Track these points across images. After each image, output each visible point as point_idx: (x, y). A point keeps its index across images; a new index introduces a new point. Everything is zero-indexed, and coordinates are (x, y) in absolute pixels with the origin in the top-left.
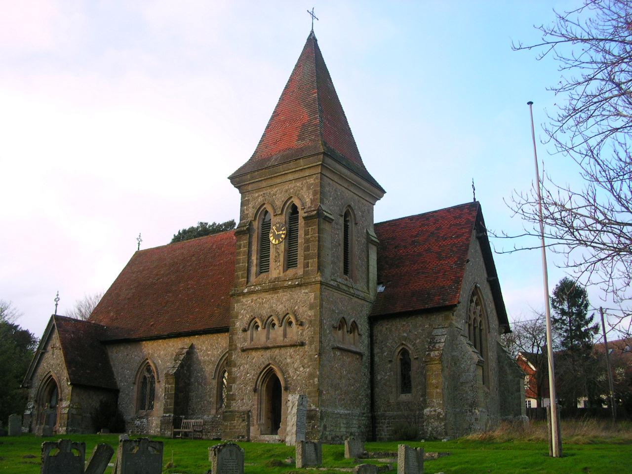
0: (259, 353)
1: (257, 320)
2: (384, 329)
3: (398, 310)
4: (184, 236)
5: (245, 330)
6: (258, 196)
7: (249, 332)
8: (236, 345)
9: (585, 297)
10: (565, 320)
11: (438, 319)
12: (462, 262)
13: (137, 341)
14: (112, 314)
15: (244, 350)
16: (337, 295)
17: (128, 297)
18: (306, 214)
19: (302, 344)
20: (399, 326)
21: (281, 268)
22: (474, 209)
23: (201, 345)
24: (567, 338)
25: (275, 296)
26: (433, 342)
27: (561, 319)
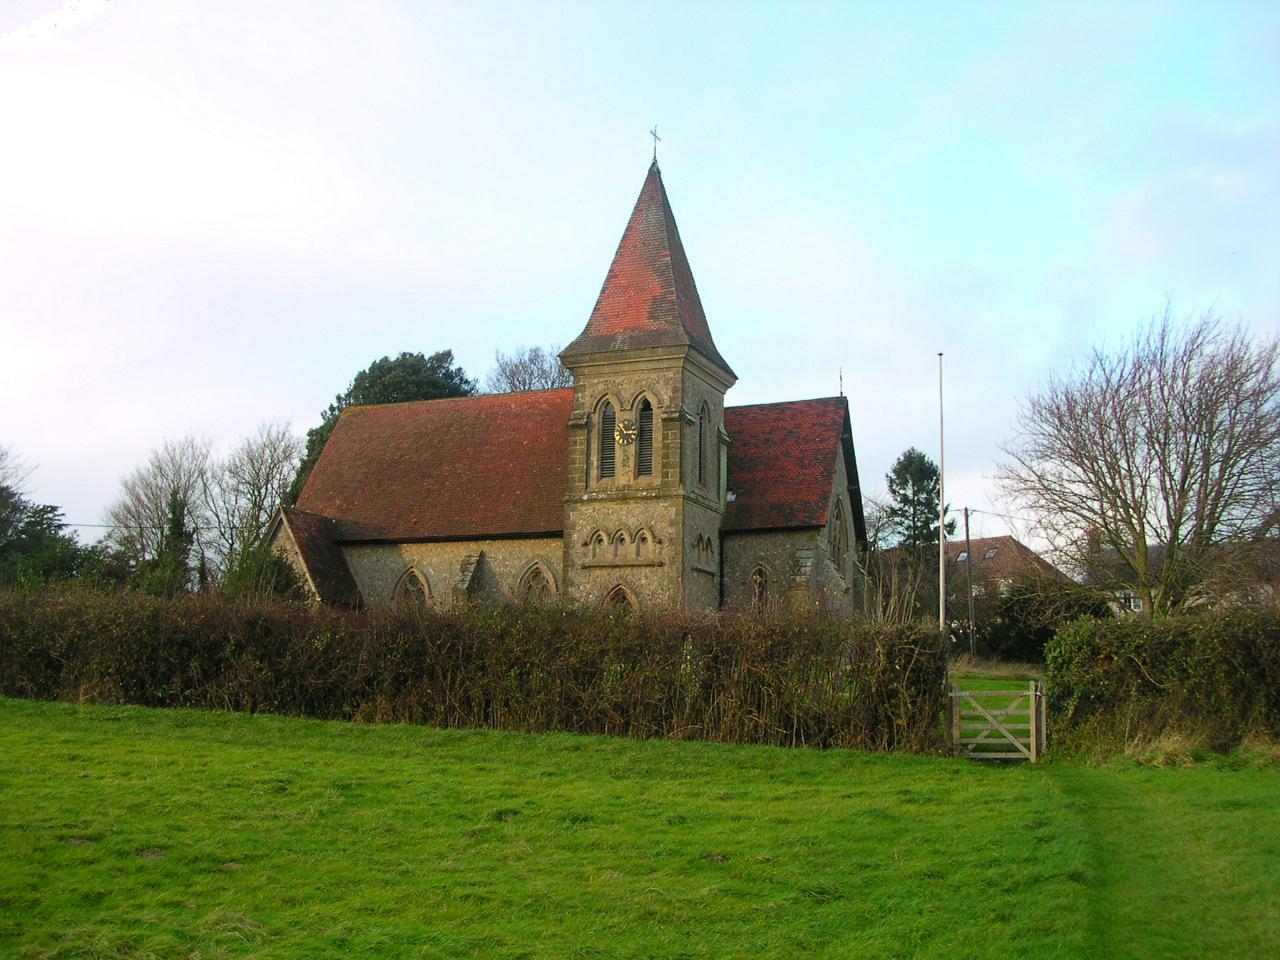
0: (605, 572)
1: (601, 533)
2: (737, 546)
3: (756, 525)
4: (375, 367)
5: (586, 544)
6: (599, 383)
7: (591, 547)
8: (572, 561)
9: (938, 479)
10: (906, 511)
11: (802, 539)
12: (829, 474)
13: (395, 543)
14: (338, 502)
15: (584, 567)
16: (696, 508)
17: (360, 477)
18: (665, 416)
19: (661, 565)
20: (755, 544)
21: (631, 474)
22: (840, 404)
23: (495, 553)
24: (909, 537)
25: (625, 507)
26: (797, 565)
27: (901, 509)
